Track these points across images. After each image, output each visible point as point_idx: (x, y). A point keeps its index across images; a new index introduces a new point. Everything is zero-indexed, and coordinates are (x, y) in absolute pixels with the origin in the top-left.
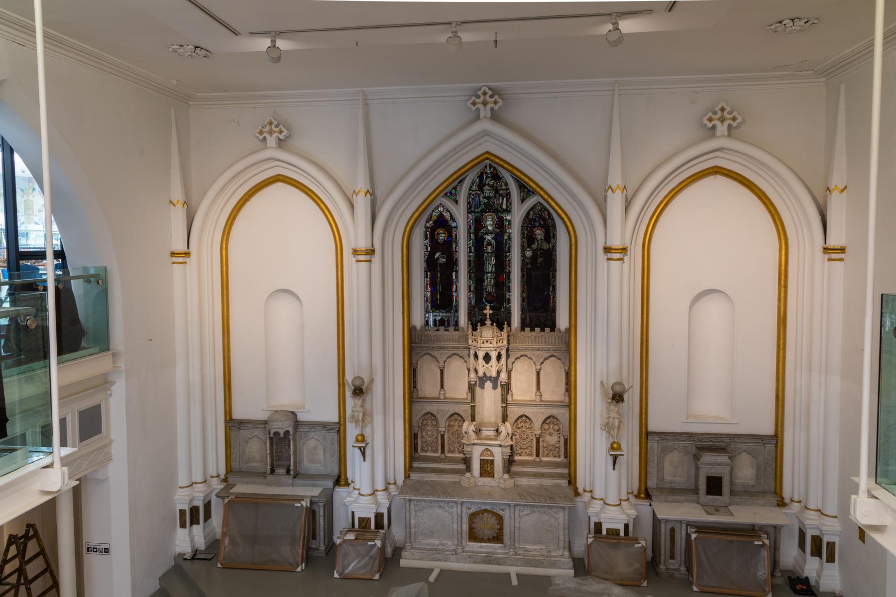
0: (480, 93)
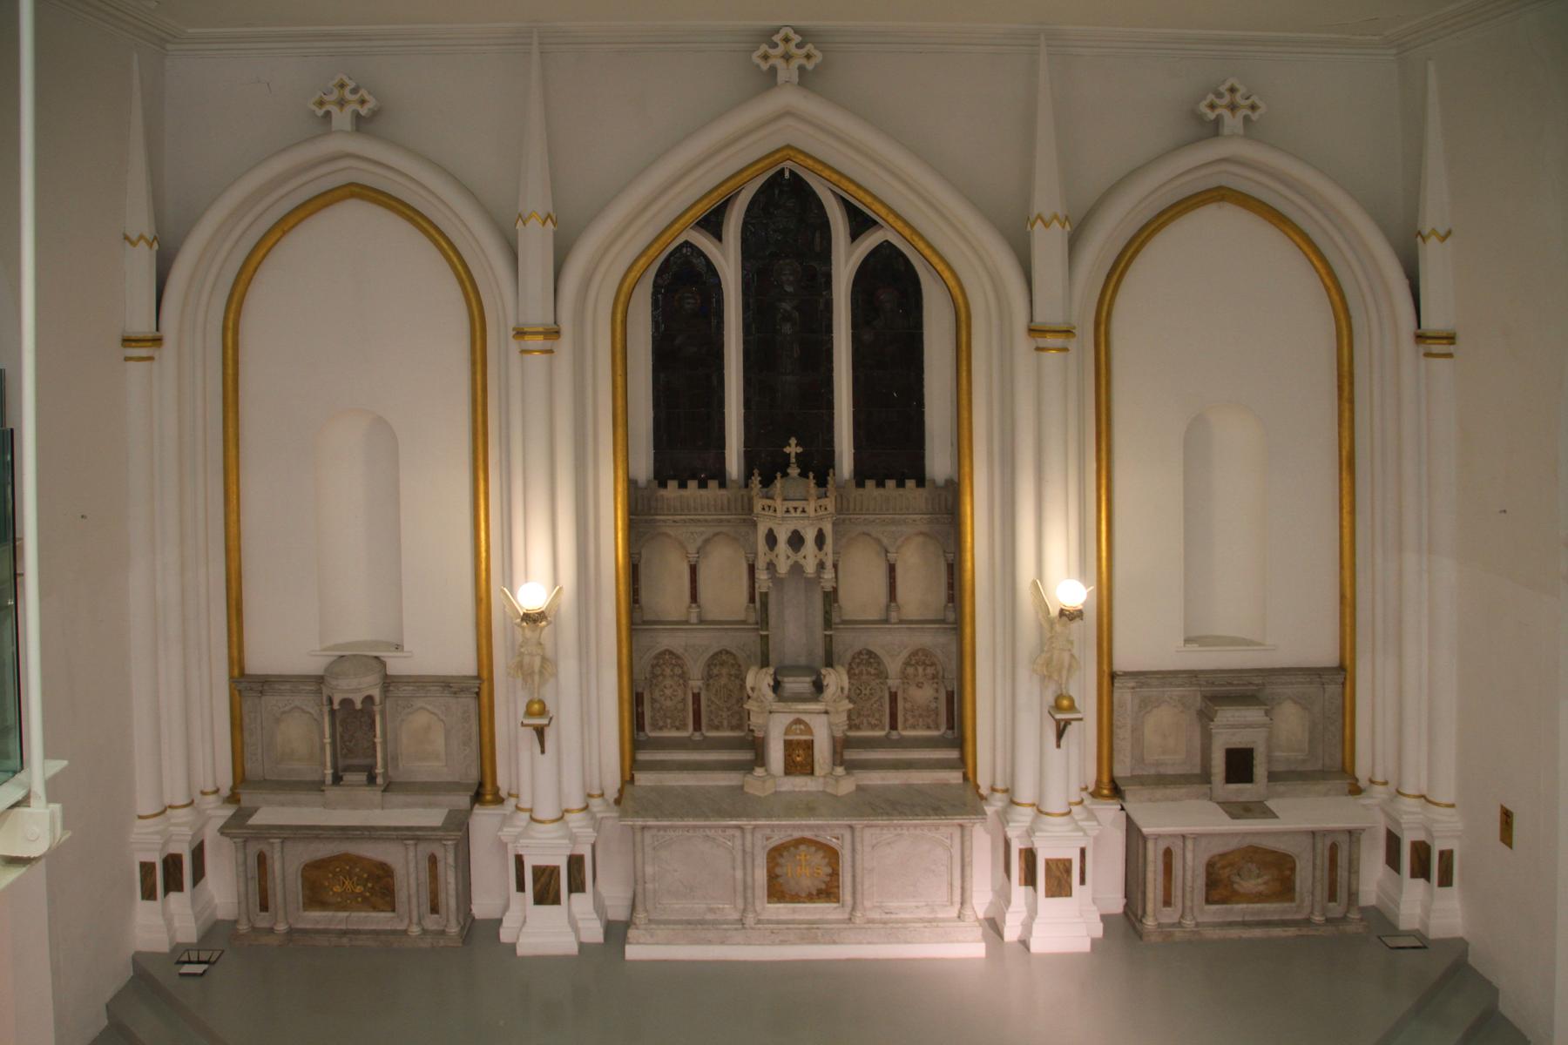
0: (776, 38)
